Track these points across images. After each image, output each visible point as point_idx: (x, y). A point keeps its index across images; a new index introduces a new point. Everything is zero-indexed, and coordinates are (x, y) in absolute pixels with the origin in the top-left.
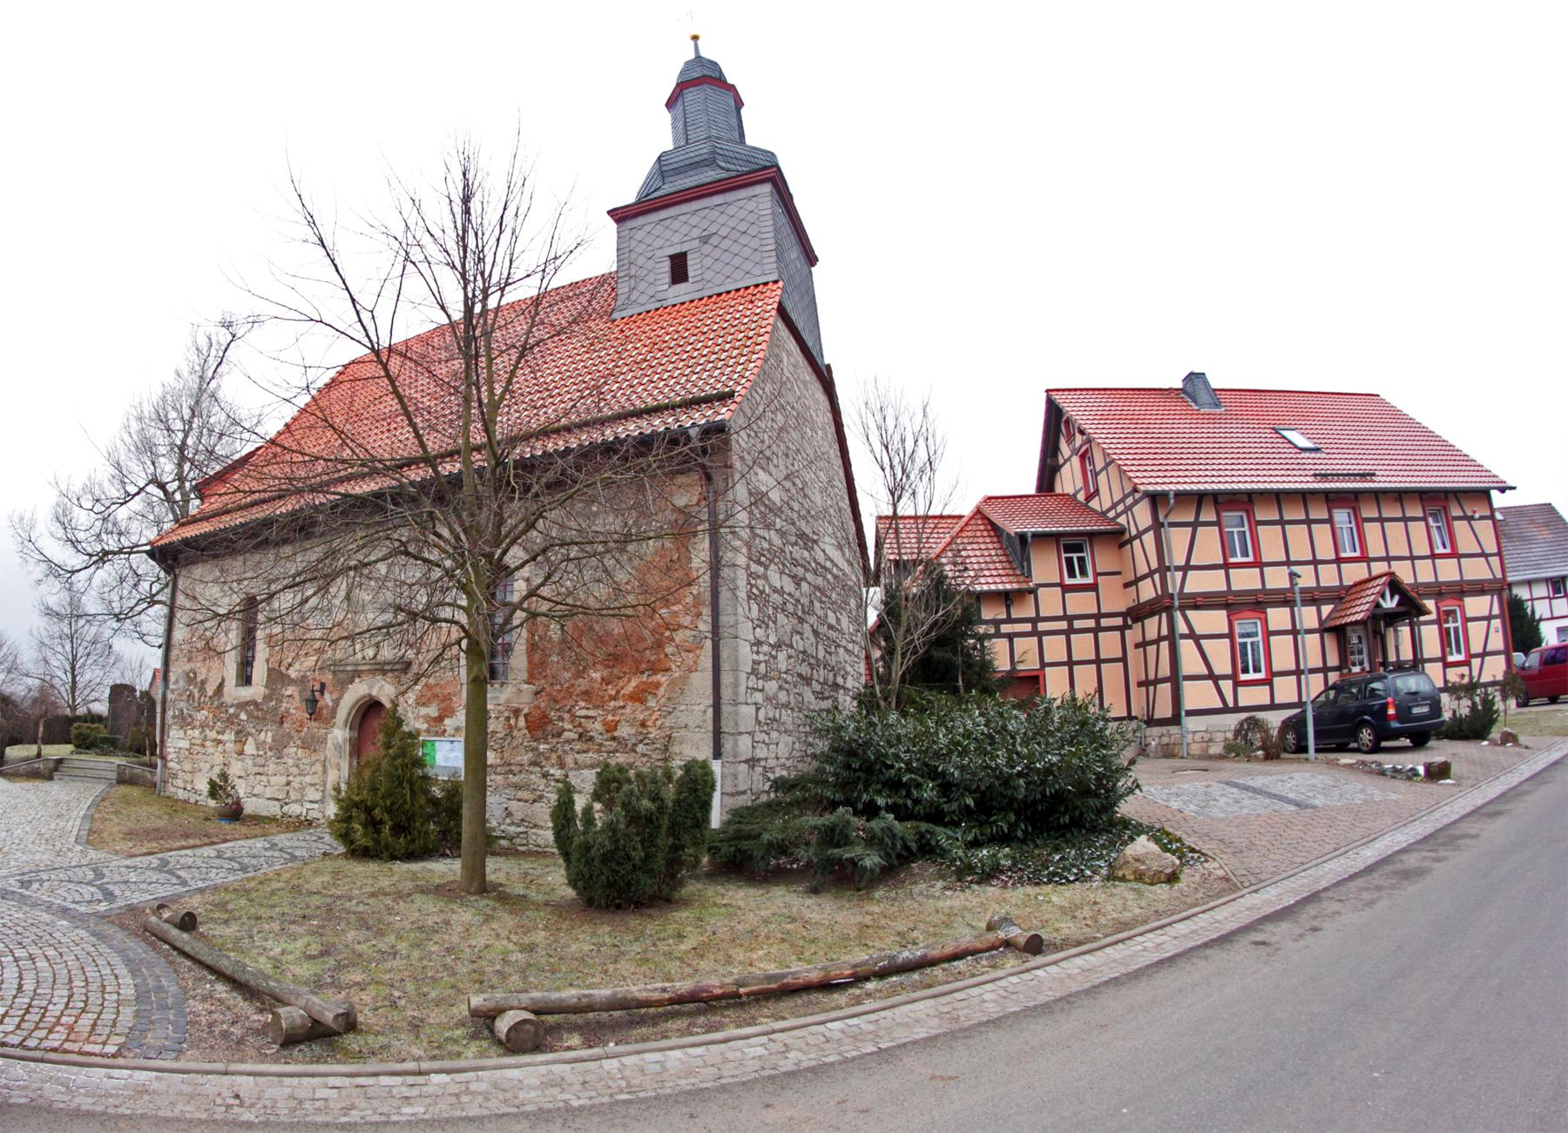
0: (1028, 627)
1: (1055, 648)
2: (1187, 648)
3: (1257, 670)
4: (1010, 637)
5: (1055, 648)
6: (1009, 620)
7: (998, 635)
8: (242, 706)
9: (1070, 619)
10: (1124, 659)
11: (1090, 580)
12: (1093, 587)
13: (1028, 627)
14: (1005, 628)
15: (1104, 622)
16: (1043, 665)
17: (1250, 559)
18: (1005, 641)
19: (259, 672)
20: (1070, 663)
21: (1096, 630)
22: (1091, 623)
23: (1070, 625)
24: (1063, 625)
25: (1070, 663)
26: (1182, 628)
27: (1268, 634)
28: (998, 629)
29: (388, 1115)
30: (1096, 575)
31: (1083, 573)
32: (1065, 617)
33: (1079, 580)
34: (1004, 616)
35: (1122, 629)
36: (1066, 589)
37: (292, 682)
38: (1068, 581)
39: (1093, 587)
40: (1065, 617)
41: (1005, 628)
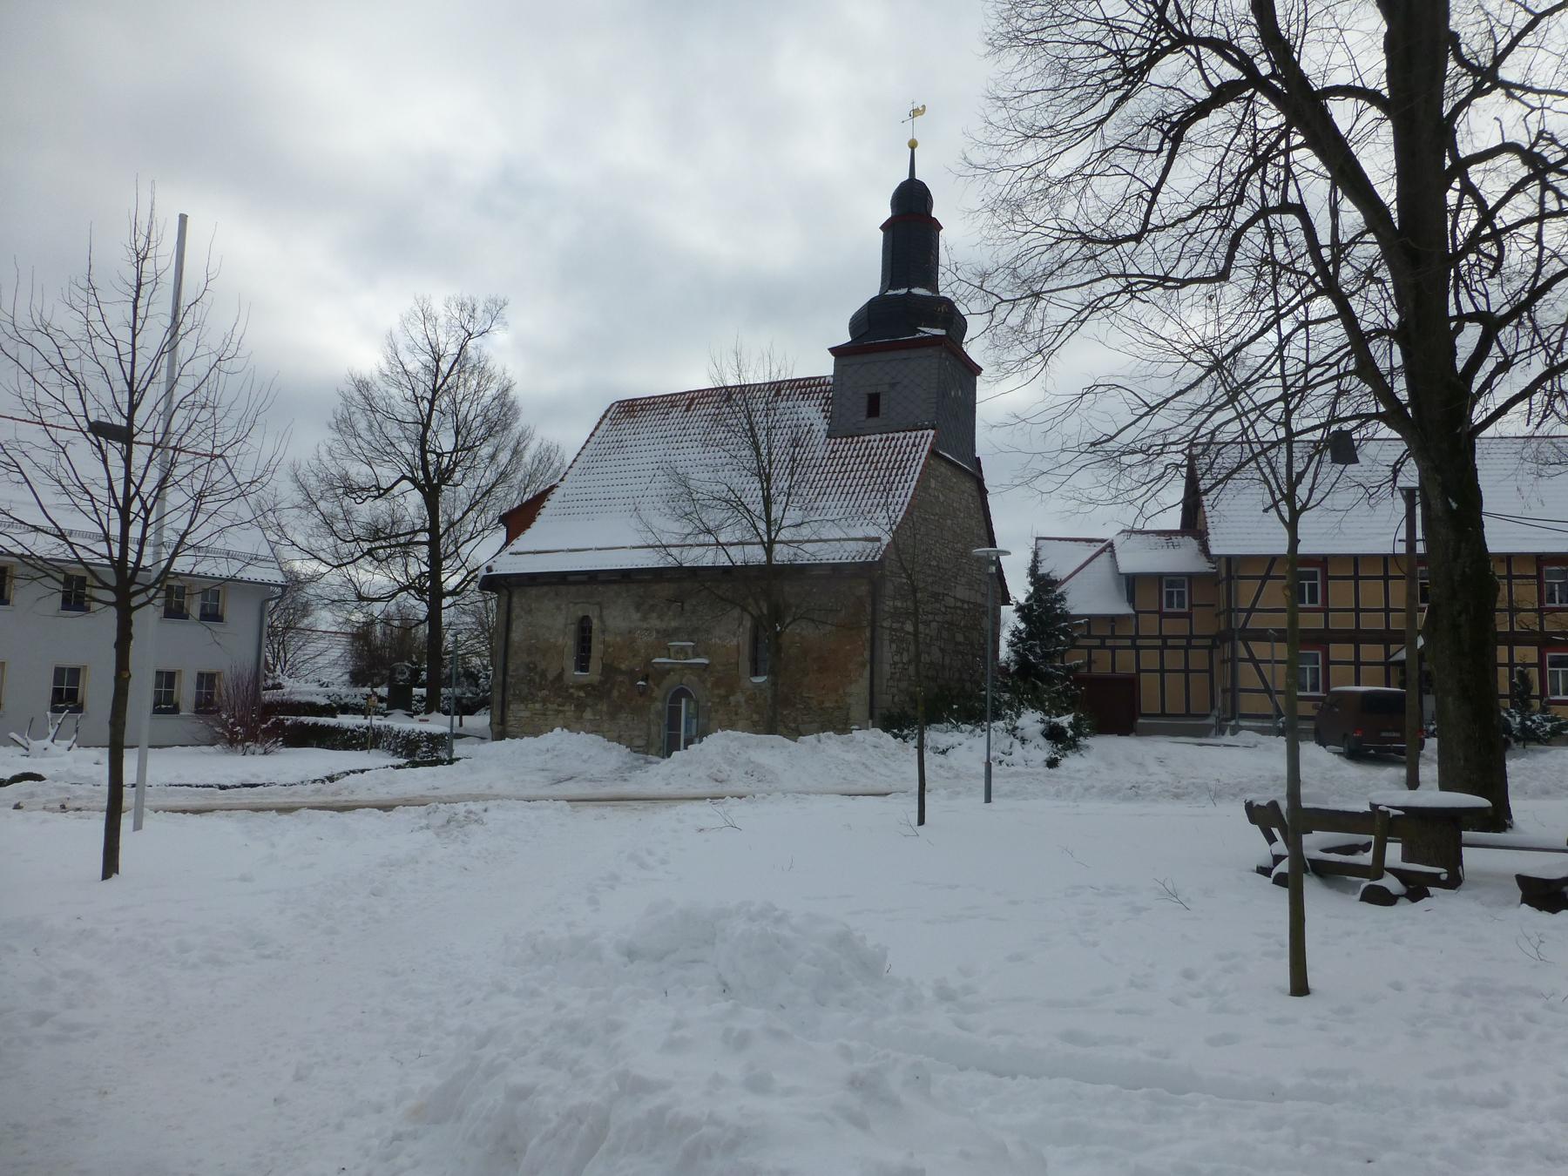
0: (1128, 642)
1: (1150, 659)
2: (1246, 669)
3: (1315, 687)
4: (1113, 649)
5: (1150, 659)
6: (1114, 637)
7: (1103, 646)
8: (581, 687)
9: (1165, 638)
10: (1210, 671)
11: (1186, 609)
12: (1188, 616)
13: (1128, 642)
14: (1109, 642)
15: (1194, 642)
16: (1139, 671)
17: (1319, 605)
18: (1108, 653)
19: (595, 664)
20: (1187, 671)
21: (1186, 649)
22: (1183, 642)
23: (1165, 642)
24: (1159, 642)
25: (1187, 671)
26: (1243, 653)
27: (1328, 663)
28: (1103, 643)
29: (67, 790)
30: (1191, 606)
31: (1181, 605)
32: (1160, 636)
33: (1175, 609)
34: (1109, 633)
35: (1211, 649)
36: (1163, 615)
37: (622, 672)
38: (1165, 609)
39: (1188, 616)
40: (1160, 636)
41: (1109, 642)
